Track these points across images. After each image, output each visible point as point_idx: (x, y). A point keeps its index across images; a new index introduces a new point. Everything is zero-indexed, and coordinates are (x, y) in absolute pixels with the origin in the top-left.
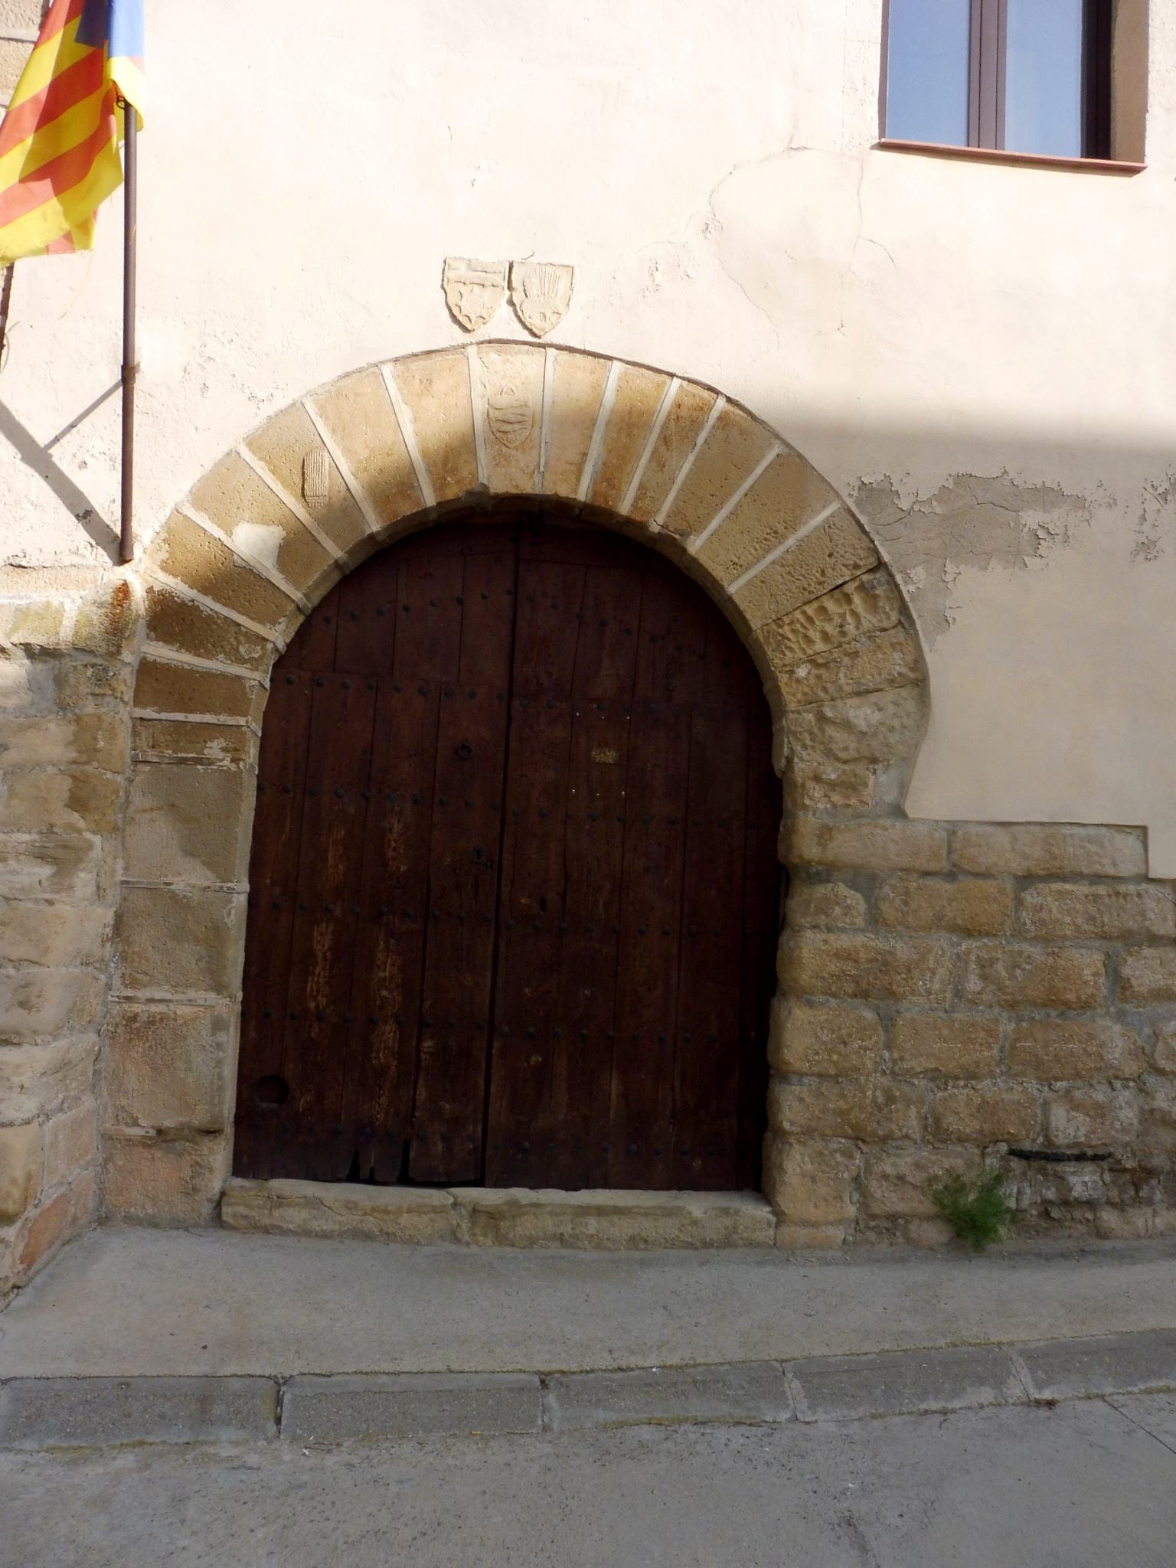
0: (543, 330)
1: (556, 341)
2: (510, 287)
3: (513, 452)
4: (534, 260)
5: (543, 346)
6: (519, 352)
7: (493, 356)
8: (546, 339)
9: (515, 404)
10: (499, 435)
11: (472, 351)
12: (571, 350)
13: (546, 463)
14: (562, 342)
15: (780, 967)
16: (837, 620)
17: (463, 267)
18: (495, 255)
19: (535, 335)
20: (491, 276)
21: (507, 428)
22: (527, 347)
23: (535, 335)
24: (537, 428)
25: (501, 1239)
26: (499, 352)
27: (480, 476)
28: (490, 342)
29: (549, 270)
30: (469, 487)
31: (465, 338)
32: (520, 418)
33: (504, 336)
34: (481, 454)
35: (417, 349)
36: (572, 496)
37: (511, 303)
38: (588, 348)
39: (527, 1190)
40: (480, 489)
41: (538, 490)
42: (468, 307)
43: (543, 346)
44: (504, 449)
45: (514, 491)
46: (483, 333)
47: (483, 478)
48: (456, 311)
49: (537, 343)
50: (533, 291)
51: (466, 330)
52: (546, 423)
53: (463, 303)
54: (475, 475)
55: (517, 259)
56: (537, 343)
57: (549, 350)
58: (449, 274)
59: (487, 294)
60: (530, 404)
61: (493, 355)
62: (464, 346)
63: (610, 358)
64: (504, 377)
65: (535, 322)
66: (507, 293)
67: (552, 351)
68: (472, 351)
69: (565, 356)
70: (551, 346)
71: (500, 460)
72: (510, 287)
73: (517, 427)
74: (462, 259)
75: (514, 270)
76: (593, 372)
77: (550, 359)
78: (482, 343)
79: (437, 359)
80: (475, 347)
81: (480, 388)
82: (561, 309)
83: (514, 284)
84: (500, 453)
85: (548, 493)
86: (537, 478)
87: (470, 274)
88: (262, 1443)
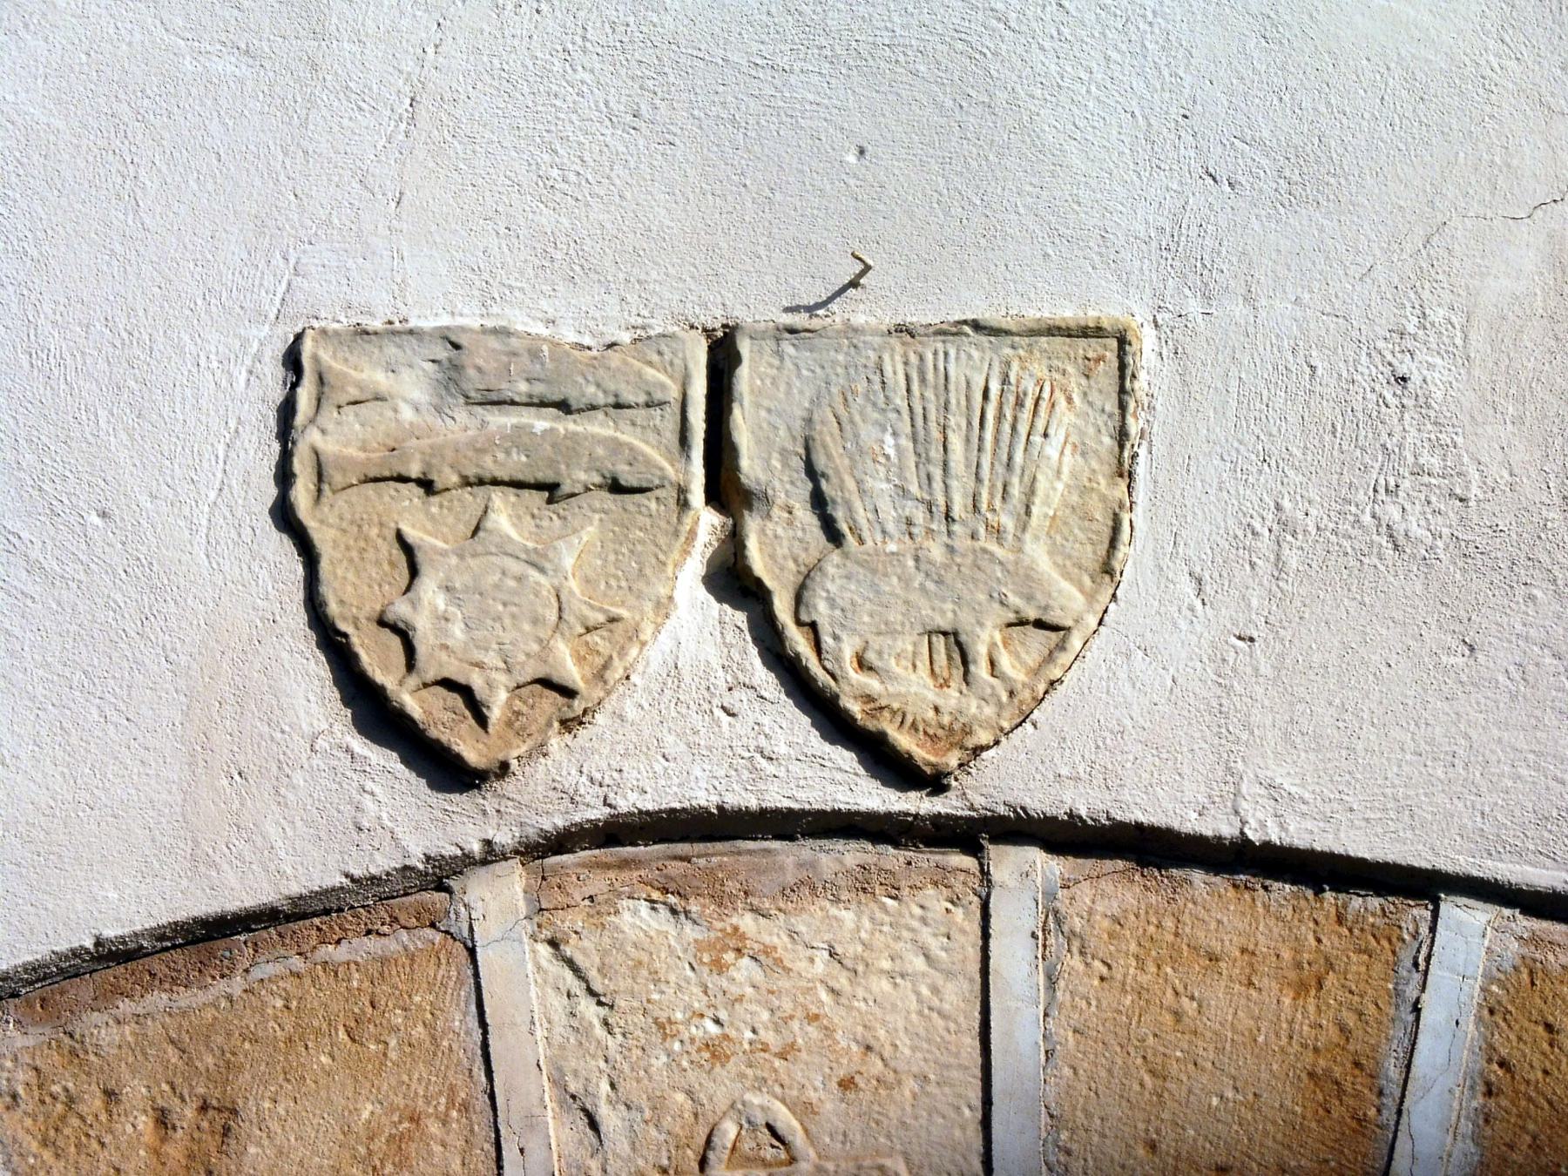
1: (1041, 801)
2: (726, 489)
4: (860, 312)
5: (969, 835)
6: (809, 886)
7: (639, 920)
8: (985, 788)
11: (496, 901)
12: (1150, 848)
14: (1087, 801)
15: (730, 434)
16: (768, 1065)
17: (411, 386)
18: (601, 290)
20: (597, 427)
22: (853, 853)
26: (672, 895)
29: (971, 365)
35: (128, 910)
37: (733, 580)
38: (1264, 828)
42: (455, 627)
43: (969, 835)
46: (564, 779)
48: (378, 660)
49: (922, 818)
50: (874, 495)
51: (446, 771)
53: (427, 608)
55: (754, 307)
56: (922, 818)
58: (330, 436)
59: (581, 542)
62: (440, 875)
63: (1425, 886)
64: (715, 1052)
65: (904, 690)
66: (708, 522)
67: (1021, 871)
69: (1108, 893)
72: (726, 489)
74: (400, 333)
75: (744, 379)
76: (1308, 983)
77: (1015, 917)
78: (561, 842)
79: (270, 966)
80: (513, 881)
82: (1068, 598)
83: (751, 466)
87: (462, 424)
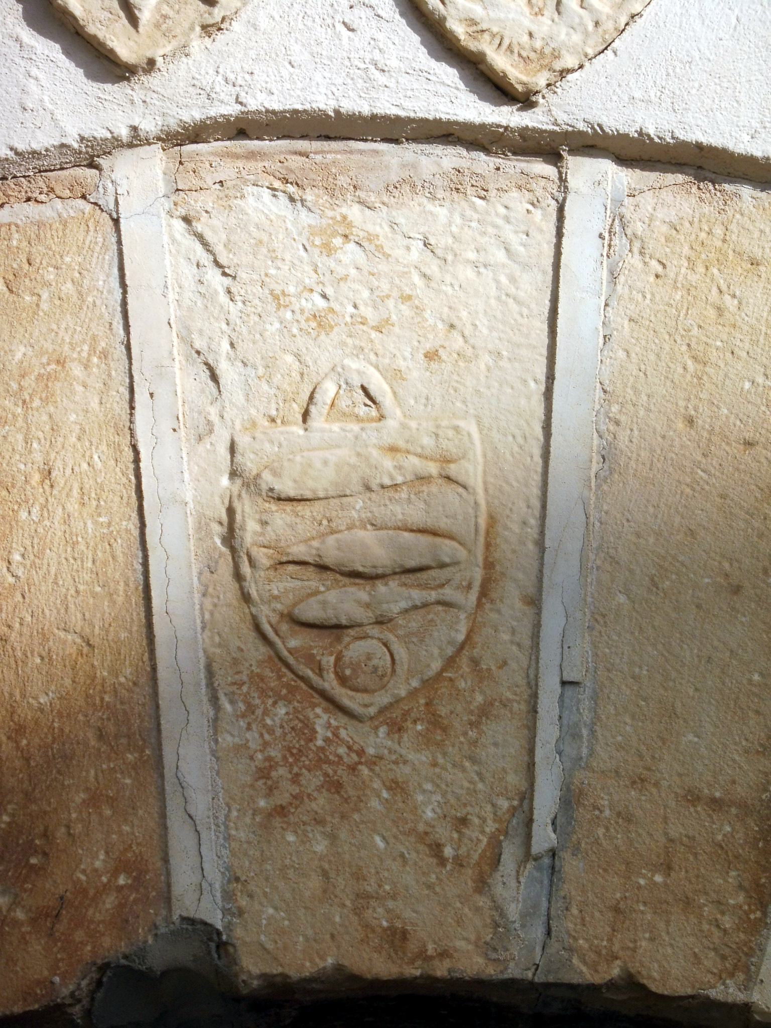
0: (545, 57)
1: (618, 120)
3: (376, 741)
5: (549, 147)
6: (408, 184)
7: (261, 205)
9: (388, 468)
10: (294, 641)
11: (139, 179)
13: (570, 799)
19: (498, 89)
21: (346, 601)
22: (450, 157)
23: (498, 89)
24: (511, 604)
25: (119, 217)
26: (291, 186)
27: (184, 880)
28: (242, 128)
30: (112, 946)
31: (98, 110)
32: (419, 549)
33: (321, 96)
34: (190, 757)
36: (729, 992)
39: (73, 64)
40: (183, 954)
41: (522, 958)
43: (549, 147)
44: (322, 720)
45: (379, 965)
47: (196, 886)
49: (511, 128)
51: (103, 64)
52: (563, 573)
54: (147, 874)
56: (511, 128)
57: (584, 171)
60: (473, 471)
61: (257, 206)
62: (92, 155)
64: (321, 322)
68: (139, 179)
69: (669, 200)
70: (593, 144)
71: (300, 781)
73: (395, 596)
77: (586, 220)
78: (196, 133)
81: (187, 381)
84: (299, 745)
85: (583, 972)
86: (513, 889)
88: (224, 937)
